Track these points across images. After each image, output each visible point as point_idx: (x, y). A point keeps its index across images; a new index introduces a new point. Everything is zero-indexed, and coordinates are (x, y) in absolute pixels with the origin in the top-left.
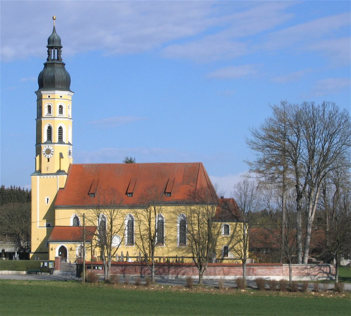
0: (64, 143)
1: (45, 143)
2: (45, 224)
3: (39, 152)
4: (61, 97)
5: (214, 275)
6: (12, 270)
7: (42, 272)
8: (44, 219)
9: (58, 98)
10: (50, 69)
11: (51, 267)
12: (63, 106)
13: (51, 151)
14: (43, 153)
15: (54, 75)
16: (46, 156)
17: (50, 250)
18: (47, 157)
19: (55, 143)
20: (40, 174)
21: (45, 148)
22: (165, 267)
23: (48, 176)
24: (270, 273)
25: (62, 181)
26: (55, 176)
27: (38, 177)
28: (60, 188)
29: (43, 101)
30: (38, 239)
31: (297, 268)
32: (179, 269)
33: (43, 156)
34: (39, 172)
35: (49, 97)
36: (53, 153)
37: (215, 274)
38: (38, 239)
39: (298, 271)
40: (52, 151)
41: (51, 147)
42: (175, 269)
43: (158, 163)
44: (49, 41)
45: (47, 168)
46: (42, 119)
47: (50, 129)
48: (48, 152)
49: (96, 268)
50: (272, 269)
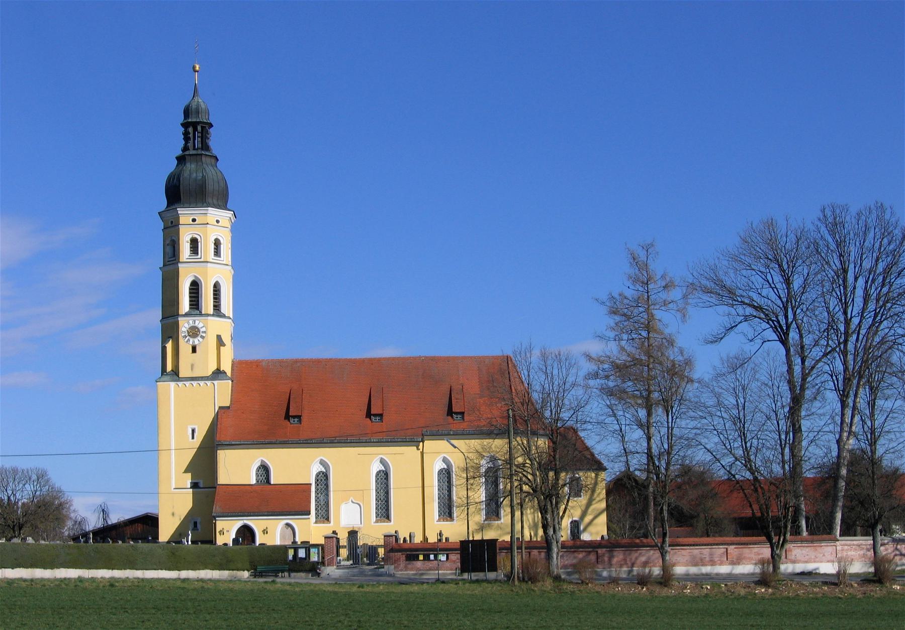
0: (224, 316)
1: (186, 315)
2: (188, 480)
3: (170, 331)
4: (218, 221)
5: (712, 565)
6: (221, 567)
7: (291, 570)
8: (186, 471)
9: (209, 225)
10: (193, 166)
11: (314, 557)
12: (222, 241)
13: (199, 331)
14: (181, 335)
15: (203, 177)
16: (189, 340)
17: (218, 534)
18: (191, 343)
19: (208, 315)
20: (176, 377)
21: (186, 325)
22: (600, 551)
23: (195, 383)
24: (816, 557)
25: (222, 393)
26: (209, 383)
28: (220, 408)
29: (182, 228)
30: (173, 514)
31: (859, 546)
32: (634, 555)
33: (182, 341)
34: (175, 374)
35: (194, 220)
37: (713, 563)
38: (173, 514)
39: (862, 552)
40: (202, 330)
41: (199, 323)
42: (624, 554)
43: (420, 357)
44: (187, 112)
45: (192, 366)
46: (180, 265)
47: (195, 287)
48: (194, 332)
49: (432, 557)
50: (818, 549)
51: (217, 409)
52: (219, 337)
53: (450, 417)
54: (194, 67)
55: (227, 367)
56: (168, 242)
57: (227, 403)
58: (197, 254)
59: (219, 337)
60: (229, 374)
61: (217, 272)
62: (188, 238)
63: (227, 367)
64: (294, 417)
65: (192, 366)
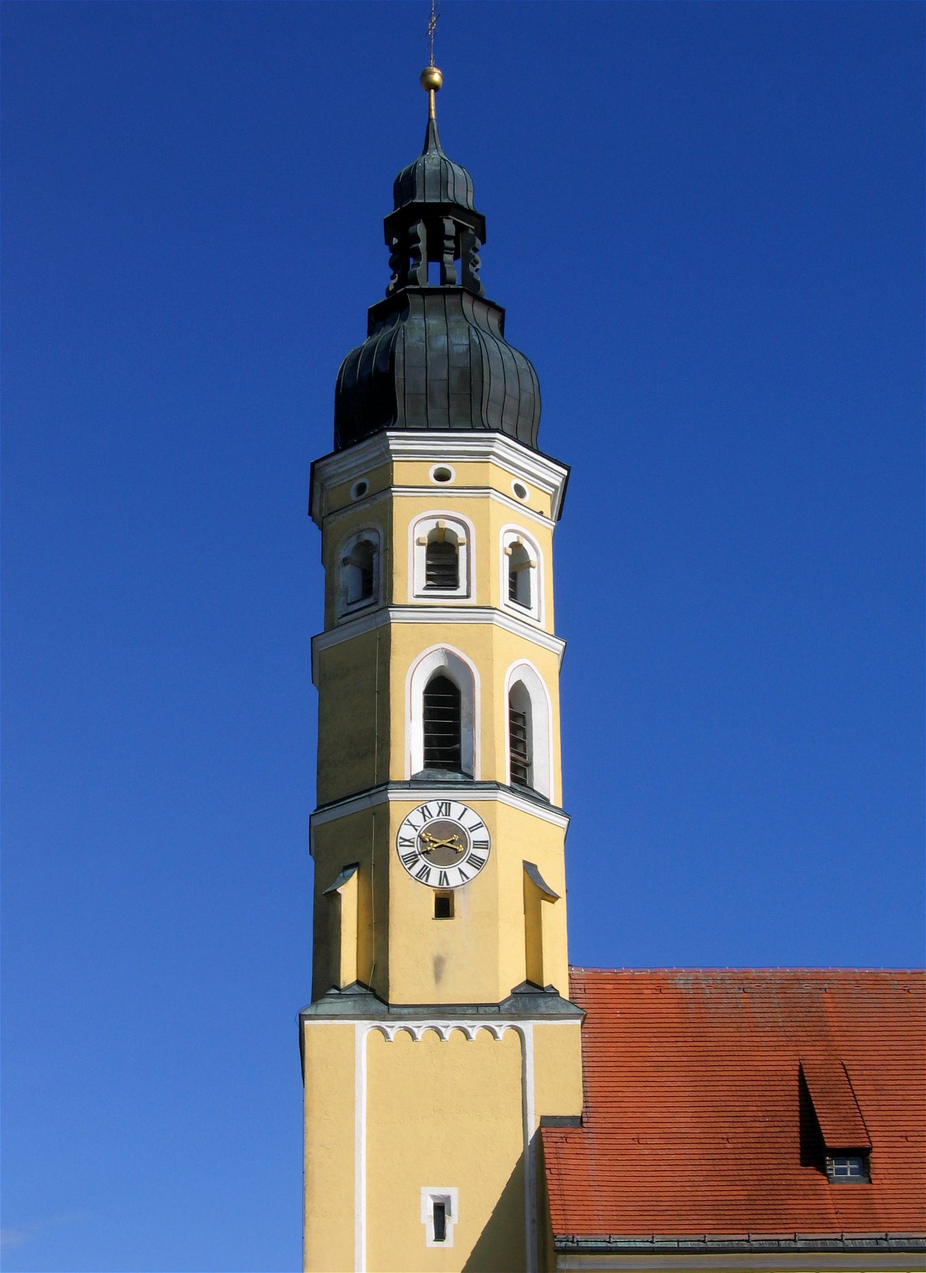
0: (542, 801)
1: (415, 783)
4: (520, 491)
13: (464, 841)
18: (434, 880)
19: (498, 786)
20: (376, 1005)
21: (416, 818)
23: (449, 1027)
25: (552, 1068)
26: (503, 1028)
27: (364, 1029)
29: (401, 505)
33: (400, 878)
34: (374, 993)
35: (442, 476)
36: (481, 853)
41: (464, 809)
45: (439, 964)
46: (393, 614)
47: (446, 700)
48: (445, 843)
51: (533, 1126)
52: (530, 869)
53: (811, 1170)
54: (425, 75)
55: (557, 974)
56: (343, 553)
57: (573, 1106)
58: (455, 585)
59: (530, 869)
60: (565, 994)
61: (519, 652)
62: (424, 531)
63: (557, 974)
64: (842, 1154)
65: (439, 964)
